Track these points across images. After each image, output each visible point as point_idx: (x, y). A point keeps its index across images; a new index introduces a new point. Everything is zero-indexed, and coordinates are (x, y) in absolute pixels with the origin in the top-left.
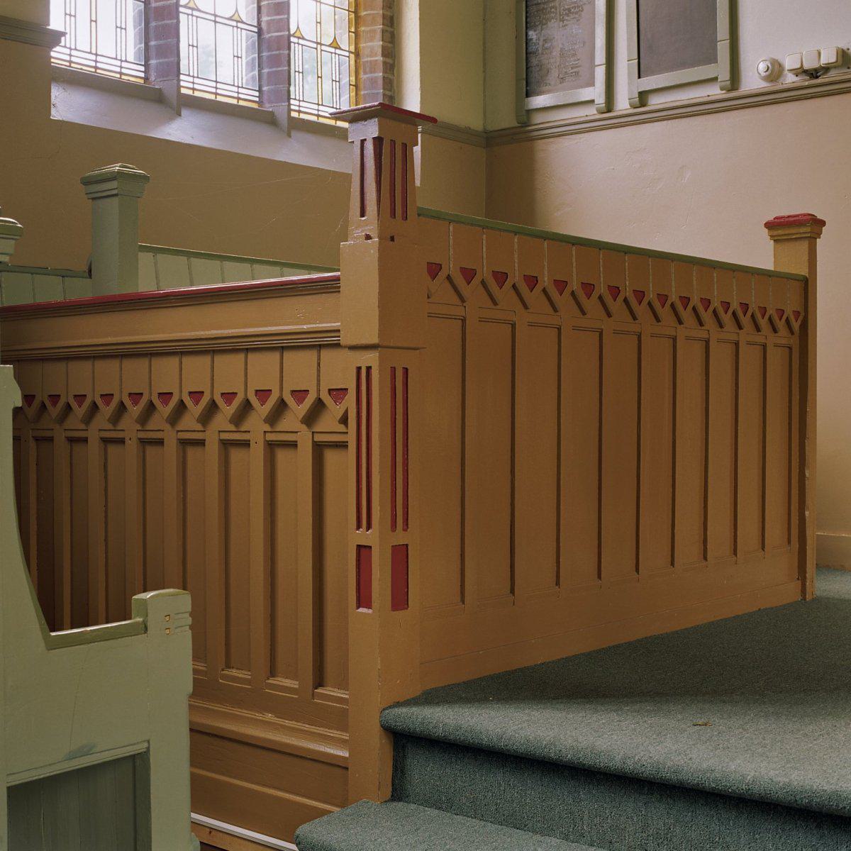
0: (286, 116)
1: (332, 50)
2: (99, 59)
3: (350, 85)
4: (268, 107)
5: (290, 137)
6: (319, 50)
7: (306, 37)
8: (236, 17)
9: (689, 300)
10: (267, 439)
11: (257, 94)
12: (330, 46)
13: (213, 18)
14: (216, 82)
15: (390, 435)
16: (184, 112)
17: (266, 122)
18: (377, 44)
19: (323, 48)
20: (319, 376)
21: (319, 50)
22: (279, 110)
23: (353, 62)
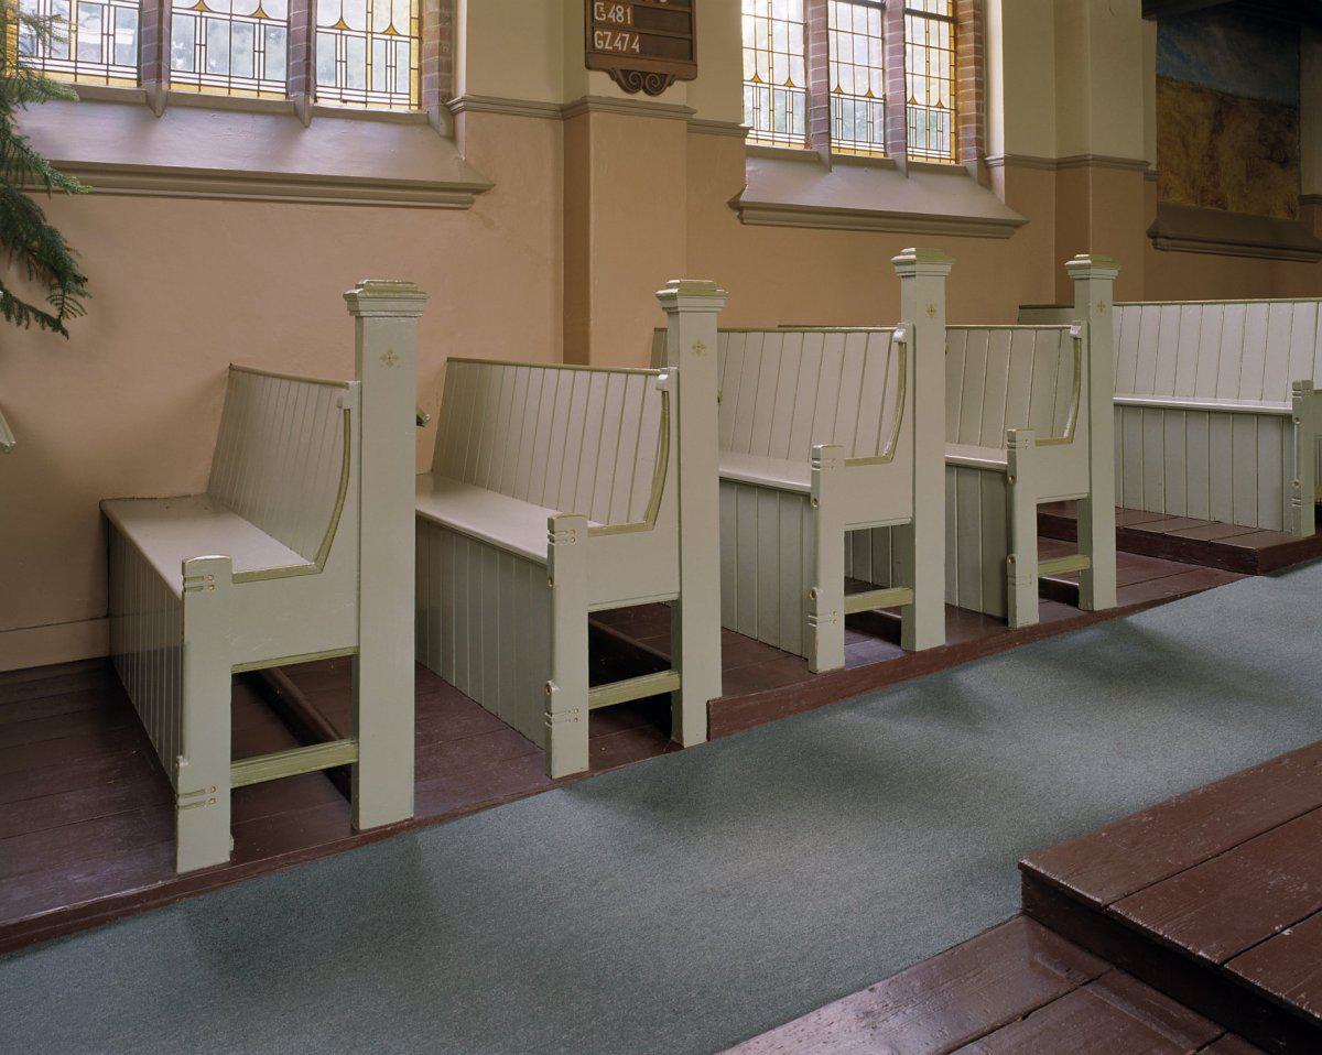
0: (904, 161)
1: (937, 109)
2: (79, 65)
3: (411, 69)
4: (891, 156)
5: (908, 177)
6: (369, 38)
7: (271, 17)
8: (756, 79)
9: (721, 445)
10: (675, 676)
11: (318, 94)
12: (751, 81)
13: (228, 17)
14: (230, 76)
15: (29, 959)
16: (834, 168)
17: (960, 175)
18: (972, 103)
19: (375, 36)
20: (680, 522)
21: (369, 38)
22: (823, 151)
23: (953, 116)
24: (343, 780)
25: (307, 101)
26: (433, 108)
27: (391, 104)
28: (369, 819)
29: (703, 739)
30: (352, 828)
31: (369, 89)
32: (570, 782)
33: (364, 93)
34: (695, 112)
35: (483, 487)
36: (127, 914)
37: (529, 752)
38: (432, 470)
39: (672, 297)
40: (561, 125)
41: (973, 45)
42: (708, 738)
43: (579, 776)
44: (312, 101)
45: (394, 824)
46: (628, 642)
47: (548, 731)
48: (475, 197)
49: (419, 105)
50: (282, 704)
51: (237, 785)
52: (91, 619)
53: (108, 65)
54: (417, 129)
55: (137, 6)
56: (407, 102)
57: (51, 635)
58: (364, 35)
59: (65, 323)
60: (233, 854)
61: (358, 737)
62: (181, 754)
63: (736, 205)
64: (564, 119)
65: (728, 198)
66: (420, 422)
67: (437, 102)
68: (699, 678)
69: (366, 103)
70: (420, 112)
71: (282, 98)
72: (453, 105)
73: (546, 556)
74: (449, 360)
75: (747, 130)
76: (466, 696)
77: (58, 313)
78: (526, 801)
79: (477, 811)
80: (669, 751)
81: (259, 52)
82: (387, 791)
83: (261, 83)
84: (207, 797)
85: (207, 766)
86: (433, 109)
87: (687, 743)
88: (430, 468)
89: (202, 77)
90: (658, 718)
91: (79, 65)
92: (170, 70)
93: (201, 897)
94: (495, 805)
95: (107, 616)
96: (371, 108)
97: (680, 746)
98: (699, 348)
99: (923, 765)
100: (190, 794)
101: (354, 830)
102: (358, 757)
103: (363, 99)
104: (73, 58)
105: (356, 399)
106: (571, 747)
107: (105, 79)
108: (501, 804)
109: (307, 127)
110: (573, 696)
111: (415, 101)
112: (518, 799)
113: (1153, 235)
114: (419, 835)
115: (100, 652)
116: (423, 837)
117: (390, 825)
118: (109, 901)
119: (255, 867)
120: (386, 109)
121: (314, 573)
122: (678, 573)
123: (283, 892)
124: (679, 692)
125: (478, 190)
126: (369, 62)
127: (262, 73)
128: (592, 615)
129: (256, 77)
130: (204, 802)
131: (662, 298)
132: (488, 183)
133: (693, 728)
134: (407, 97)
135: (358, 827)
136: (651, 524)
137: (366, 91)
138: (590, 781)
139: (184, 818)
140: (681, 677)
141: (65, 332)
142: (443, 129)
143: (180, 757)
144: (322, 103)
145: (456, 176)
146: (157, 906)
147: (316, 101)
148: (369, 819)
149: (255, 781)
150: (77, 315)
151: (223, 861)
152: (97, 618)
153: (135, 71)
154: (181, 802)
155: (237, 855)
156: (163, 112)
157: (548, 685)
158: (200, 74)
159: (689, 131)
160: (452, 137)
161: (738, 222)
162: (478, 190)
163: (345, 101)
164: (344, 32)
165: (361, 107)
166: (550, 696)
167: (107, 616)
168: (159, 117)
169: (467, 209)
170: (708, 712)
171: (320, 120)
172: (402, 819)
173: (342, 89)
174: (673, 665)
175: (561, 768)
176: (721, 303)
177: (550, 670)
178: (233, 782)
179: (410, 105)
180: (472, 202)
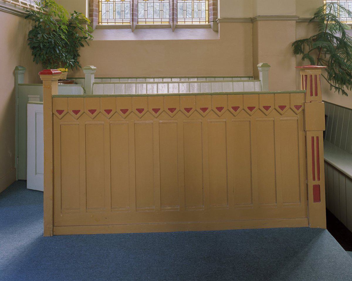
14: (154, 18)
19: (116, 2)
31: (193, 18)
33: (191, 19)
41: (212, 2)
53: (146, 19)
55: (169, 2)
58: (113, 2)
81: (146, 11)
83: (123, 20)
89: (146, 19)
91: (154, 19)
92: (138, 19)
96: (117, 24)
99: (277, 271)
104: (114, 18)
107: (107, 23)
113: (173, 31)
126: (114, 10)
127: (146, 17)
128: (319, 186)
129: (161, 18)
134: (205, 19)
137: (192, 18)
144: (179, 23)
153: (178, 21)
158: (123, 19)
164: (108, 2)
173: (123, 19)
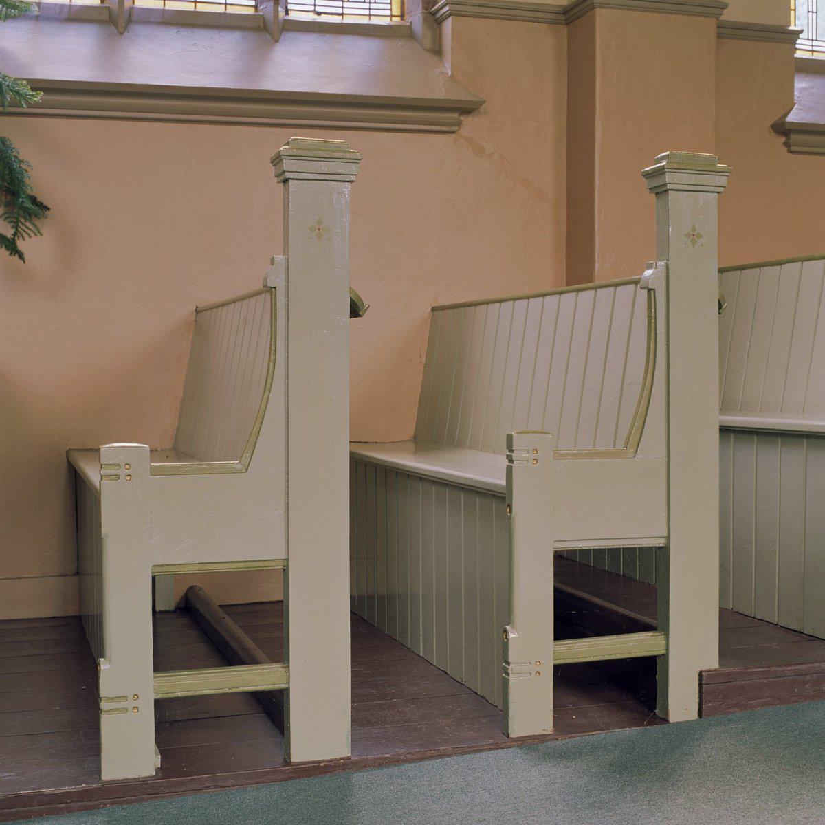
24: (272, 707)
25: (276, 12)
26: (416, 19)
27: (370, 15)
28: (301, 752)
29: (693, 715)
30: (285, 761)
32: (527, 743)
34: (724, 7)
35: (465, 448)
36: (52, 812)
37: (487, 715)
38: (415, 437)
39: (660, 172)
40: (564, 30)
42: (700, 714)
43: (542, 738)
44: (282, 14)
45: (328, 761)
46: (603, 590)
47: (505, 684)
48: (462, 118)
49: (402, 16)
50: (211, 622)
51: (160, 696)
52: (60, 576)
54: (399, 43)
56: (389, 13)
57: (20, 592)
59: (20, 244)
60: (157, 770)
61: (289, 662)
62: (102, 656)
63: (782, 129)
64: (568, 23)
65: (772, 120)
66: (355, 311)
67: (420, 10)
68: (689, 646)
69: (342, 14)
70: (402, 23)
71: (251, 11)
72: (438, 10)
73: (504, 483)
74: (434, 309)
75: (797, 34)
76: (433, 665)
77: (13, 231)
78: (477, 756)
79: (422, 759)
80: (650, 724)
82: (321, 723)
84: (129, 704)
85: (131, 677)
86: (417, 18)
87: (673, 718)
88: (412, 435)
90: (637, 686)
93: (125, 806)
94: (441, 756)
95: (77, 574)
96: (347, 20)
97: (665, 721)
98: (694, 236)
100: (112, 699)
101: (287, 762)
102: (288, 682)
103: (340, 11)
105: (283, 276)
106: (531, 704)
108: (449, 756)
109: (277, 41)
110: (534, 650)
111: (397, 11)
112: (470, 753)
114: (355, 775)
115: (71, 611)
116: (359, 779)
117: (324, 761)
118: (35, 796)
119: (179, 784)
120: (365, 21)
121: (240, 472)
122: (665, 514)
123: (206, 809)
124: (665, 656)
125: (467, 110)
130: (127, 709)
131: (648, 175)
132: (477, 100)
133: (681, 701)
135: (290, 758)
136: (631, 451)
138: (552, 744)
139: (108, 724)
140: (667, 639)
141: (21, 256)
142: (428, 42)
143: (102, 660)
144: (294, 16)
145: (439, 91)
146: (80, 809)
147: (287, 13)
148: (301, 752)
149: (179, 695)
150: (32, 234)
151: (148, 775)
152: (67, 575)
154: (104, 705)
155: (166, 770)
156: (126, 28)
157: (505, 631)
159: (719, 36)
160: (438, 51)
161: (785, 150)
162: (467, 110)
163: (319, 14)
165: (337, 19)
166: (507, 643)
167: (77, 574)
168: (121, 34)
169: (453, 132)
170: (700, 685)
171: (291, 34)
172: (338, 757)
174: (658, 628)
175: (518, 728)
176: (723, 180)
177: (507, 615)
178: (156, 692)
179: (391, 16)
180: (459, 124)
